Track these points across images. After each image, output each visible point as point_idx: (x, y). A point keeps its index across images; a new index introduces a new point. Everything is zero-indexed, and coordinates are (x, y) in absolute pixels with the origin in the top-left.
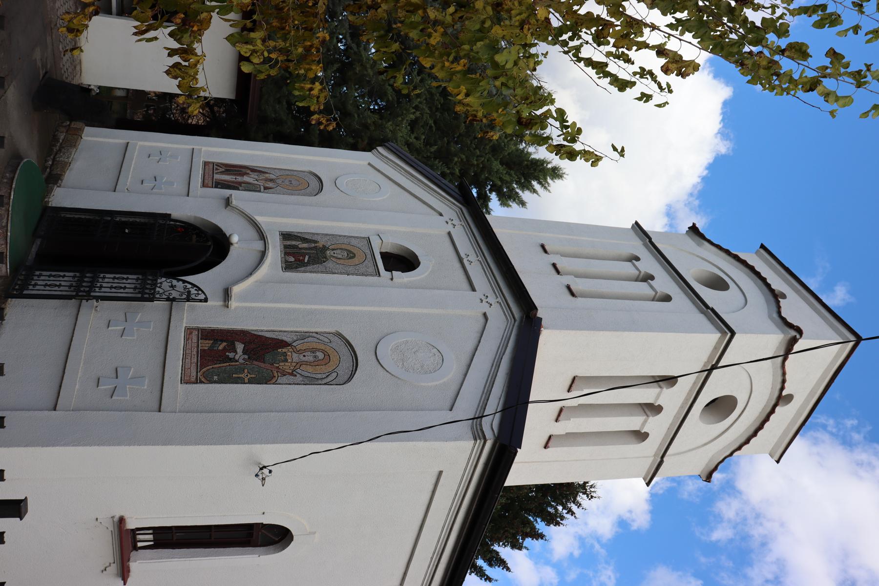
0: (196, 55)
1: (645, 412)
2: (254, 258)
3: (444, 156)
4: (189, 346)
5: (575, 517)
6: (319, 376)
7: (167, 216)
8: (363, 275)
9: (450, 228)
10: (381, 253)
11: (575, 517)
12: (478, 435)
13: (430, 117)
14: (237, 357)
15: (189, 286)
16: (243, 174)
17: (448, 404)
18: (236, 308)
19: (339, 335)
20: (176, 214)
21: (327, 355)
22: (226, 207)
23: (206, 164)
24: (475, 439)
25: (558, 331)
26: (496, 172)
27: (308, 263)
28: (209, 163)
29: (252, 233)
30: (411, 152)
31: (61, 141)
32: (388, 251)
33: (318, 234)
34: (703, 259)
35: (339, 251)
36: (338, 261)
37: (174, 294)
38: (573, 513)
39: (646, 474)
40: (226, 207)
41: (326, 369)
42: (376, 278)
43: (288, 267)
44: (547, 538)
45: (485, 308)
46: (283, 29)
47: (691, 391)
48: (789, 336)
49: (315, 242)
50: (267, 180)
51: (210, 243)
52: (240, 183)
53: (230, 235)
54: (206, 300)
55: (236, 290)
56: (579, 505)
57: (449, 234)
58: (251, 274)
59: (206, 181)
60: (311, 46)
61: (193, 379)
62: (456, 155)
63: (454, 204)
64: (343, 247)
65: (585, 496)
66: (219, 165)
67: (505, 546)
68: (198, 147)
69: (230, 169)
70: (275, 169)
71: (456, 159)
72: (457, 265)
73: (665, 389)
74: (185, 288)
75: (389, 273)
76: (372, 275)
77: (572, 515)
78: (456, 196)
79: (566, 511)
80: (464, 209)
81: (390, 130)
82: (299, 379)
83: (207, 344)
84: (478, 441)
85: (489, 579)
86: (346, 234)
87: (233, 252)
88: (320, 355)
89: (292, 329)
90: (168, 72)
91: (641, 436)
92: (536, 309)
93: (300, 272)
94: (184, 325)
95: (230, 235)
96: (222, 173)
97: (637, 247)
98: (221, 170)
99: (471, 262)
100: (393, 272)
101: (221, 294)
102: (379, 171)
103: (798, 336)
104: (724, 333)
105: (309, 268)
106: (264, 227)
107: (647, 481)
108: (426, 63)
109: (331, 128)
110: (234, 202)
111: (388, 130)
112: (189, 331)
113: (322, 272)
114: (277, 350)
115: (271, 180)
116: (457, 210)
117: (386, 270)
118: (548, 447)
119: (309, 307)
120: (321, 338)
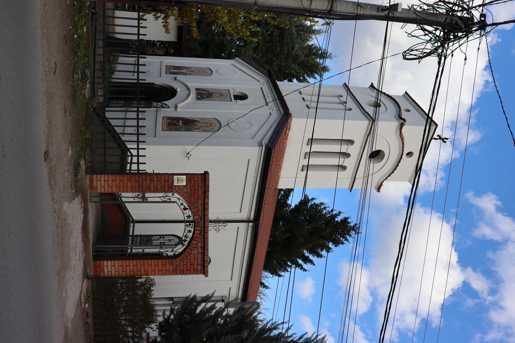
0: (168, 23)
5: (349, 242)
7: (153, 84)
9: (262, 86)
10: (233, 95)
11: (349, 242)
12: (260, 145)
14: (180, 125)
16: (181, 69)
18: (179, 111)
19: (216, 119)
20: (156, 83)
21: (211, 125)
22: (175, 80)
23: (166, 66)
24: (259, 147)
25: (299, 119)
26: (293, 68)
27: (206, 98)
28: (168, 66)
29: (185, 88)
31: (112, 60)
32: (237, 94)
33: (210, 89)
36: (217, 97)
37: (158, 106)
38: (348, 240)
39: (349, 186)
40: (175, 80)
41: (211, 128)
43: (198, 99)
45: (271, 111)
46: (187, 15)
47: (361, 147)
48: (401, 122)
49: (208, 91)
52: (180, 73)
53: (177, 89)
54: (169, 108)
56: (350, 236)
57: (261, 88)
58: (184, 101)
59: (167, 72)
62: (275, 62)
63: (265, 77)
64: (219, 92)
65: (354, 232)
66: (172, 66)
68: (163, 60)
69: (176, 68)
70: (193, 67)
72: (263, 98)
73: (349, 146)
74: (162, 104)
75: (235, 101)
76: (229, 101)
77: (347, 241)
78: (267, 75)
79: (344, 239)
81: (244, 52)
82: (201, 130)
83: (170, 121)
84: (260, 147)
85: (305, 270)
87: (178, 94)
88: (208, 124)
89: (199, 117)
90: (163, 26)
91: (344, 168)
93: (202, 100)
94: (162, 116)
95: (177, 89)
96: (173, 69)
97: (344, 92)
98: (172, 68)
99: (268, 97)
100: (237, 100)
101: (174, 107)
102: (235, 67)
103: (404, 122)
104: (370, 121)
105: (205, 99)
106: (189, 87)
107: (350, 190)
108: (437, 18)
109: (198, 38)
110: (178, 78)
112: (163, 118)
113: (210, 100)
114: (194, 122)
115: (192, 71)
116: (266, 79)
117: (235, 99)
120: (209, 120)
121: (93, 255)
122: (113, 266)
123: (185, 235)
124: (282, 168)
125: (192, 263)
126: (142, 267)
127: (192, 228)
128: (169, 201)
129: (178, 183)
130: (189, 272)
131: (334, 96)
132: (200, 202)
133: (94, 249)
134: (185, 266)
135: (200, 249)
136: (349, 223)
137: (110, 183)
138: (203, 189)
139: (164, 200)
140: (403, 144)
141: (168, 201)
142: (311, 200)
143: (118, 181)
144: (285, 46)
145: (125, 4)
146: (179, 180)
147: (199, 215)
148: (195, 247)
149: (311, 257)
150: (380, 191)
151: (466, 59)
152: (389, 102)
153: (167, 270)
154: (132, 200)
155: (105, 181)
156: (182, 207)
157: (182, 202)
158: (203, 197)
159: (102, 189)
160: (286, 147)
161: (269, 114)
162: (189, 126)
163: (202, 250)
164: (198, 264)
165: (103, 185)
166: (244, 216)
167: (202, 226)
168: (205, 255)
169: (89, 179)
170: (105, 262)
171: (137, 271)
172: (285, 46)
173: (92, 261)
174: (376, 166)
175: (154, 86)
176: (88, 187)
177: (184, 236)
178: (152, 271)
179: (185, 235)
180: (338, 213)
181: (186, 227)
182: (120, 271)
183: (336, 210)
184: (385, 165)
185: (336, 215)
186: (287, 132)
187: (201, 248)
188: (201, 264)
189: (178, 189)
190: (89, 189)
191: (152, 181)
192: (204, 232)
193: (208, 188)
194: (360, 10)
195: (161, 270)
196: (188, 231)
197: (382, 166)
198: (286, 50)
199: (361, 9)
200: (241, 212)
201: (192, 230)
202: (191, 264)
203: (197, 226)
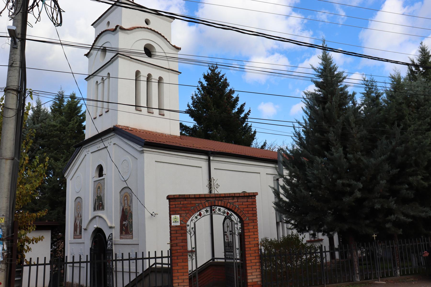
1: (151, 79)
2: (101, 220)
3: (68, 146)
4: (128, 238)
5: (224, 74)
6: (130, 198)
8: (104, 184)
9: (90, 153)
10: (99, 177)
11: (224, 74)
12: (142, 152)
13: (53, 152)
14: (127, 223)
15: (109, 239)
16: (77, 225)
17: (136, 159)
23: (74, 238)
24: (144, 153)
27: (102, 202)
29: (94, 221)
30: (67, 160)
32: (98, 174)
33: (94, 199)
34: (96, 54)
35: (98, 192)
37: (111, 244)
38: (223, 75)
42: (105, 180)
43: (103, 209)
44: (231, 88)
45: (112, 144)
46: (26, 222)
47: (142, 64)
49: (96, 200)
50: (78, 216)
51: (98, 234)
52: (80, 226)
53: (95, 228)
54: (112, 234)
55: (109, 225)
56: (219, 73)
57: (92, 153)
58: (105, 220)
60: (29, 216)
61: (132, 236)
62: (68, 142)
63: (82, 150)
64: (97, 190)
65: (216, 70)
66: (74, 234)
67: (237, 104)
69: (75, 230)
71: (69, 142)
72: (101, 151)
73: (141, 75)
74: (109, 240)
76: (104, 181)
77: (224, 76)
78: (79, 148)
80: (83, 147)
82: (131, 205)
83: (124, 232)
85: (249, 111)
86: (93, 189)
87: (100, 226)
88: (125, 198)
90: (37, 243)
91: (160, 80)
93: (104, 205)
95: (95, 228)
96: (77, 232)
97: (94, 80)
98: (76, 233)
99: (99, 147)
103: (119, 27)
104: (118, 57)
107: (179, 74)
110: (85, 227)
111: (59, 171)
113: (104, 197)
115: (78, 215)
117: (103, 176)
118: (164, 114)
119: (113, 202)
122: (252, 274)
123: (222, 214)
124: (162, 133)
125: (246, 206)
127: (216, 208)
128: (194, 228)
129: (178, 222)
130: (254, 208)
131: (97, 88)
134: (249, 212)
136: (208, 74)
137: (181, 281)
138: (182, 200)
139: (193, 233)
140: (138, 28)
141: (194, 230)
142: (189, 107)
143: (178, 274)
144: (52, 133)
146: (176, 221)
148: (233, 204)
149: (238, 106)
153: (254, 227)
155: (178, 286)
156: (199, 217)
157: (194, 217)
158: (190, 200)
161: (115, 145)
162: (127, 215)
164: (247, 201)
166: (204, 164)
167: (214, 199)
170: (249, 281)
171: (255, 253)
177: (224, 214)
178: (254, 241)
179: (222, 214)
180: (200, 84)
185: (202, 85)
186: (130, 129)
187: (233, 199)
189: (183, 222)
191: (177, 244)
192: (220, 197)
194: (16, 64)
196: (219, 211)
197: (158, 46)
198: (56, 132)
199: (15, 63)
200: (201, 167)
201: (218, 207)
203: (215, 203)
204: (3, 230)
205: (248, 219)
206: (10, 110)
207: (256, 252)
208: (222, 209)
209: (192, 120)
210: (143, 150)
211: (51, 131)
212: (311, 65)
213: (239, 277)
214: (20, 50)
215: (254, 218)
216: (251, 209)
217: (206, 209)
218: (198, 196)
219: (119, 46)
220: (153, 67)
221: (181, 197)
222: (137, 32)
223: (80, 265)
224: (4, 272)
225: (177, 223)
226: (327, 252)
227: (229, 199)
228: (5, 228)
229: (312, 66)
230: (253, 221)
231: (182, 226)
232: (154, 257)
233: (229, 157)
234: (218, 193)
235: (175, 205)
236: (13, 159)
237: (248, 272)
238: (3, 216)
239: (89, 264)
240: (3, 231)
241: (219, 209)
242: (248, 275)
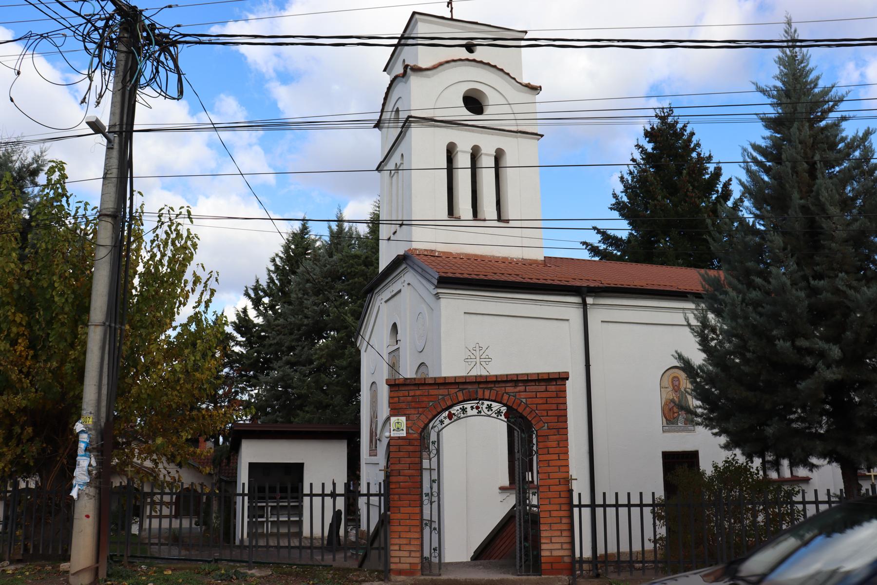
12: (438, 298)
24: (440, 298)
38: (685, 126)
57: (386, 302)
73: (458, 149)
77: (686, 127)
91: (499, 156)
92: (398, 255)
103: (409, 67)
116: (376, 296)
121: (534, 575)
122: (551, 540)
123: (495, 416)
124: (504, 256)
125: (544, 401)
126: (553, 488)
127: (483, 404)
128: (436, 443)
129: (403, 430)
130: (562, 405)
131: (392, 183)
132: (434, 392)
133: (522, 572)
134: (550, 413)
135: (518, 389)
136: (652, 128)
137: (404, 541)
138: (412, 388)
139: (435, 452)
140: (448, 62)
141: (436, 445)
142: (616, 199)
143: (400, 529)
144: (353, 269)
145: (281, 521)
146: (398, 429)
147: (456, 393)
148: (515, 396)
149: (719, 187)
150: (538, 85)
151: (170, 7)
152: (393, 95)
153: (559, 445)
154: (435, 505)
155: (400, 550)
156: (447, 421)
157: (438, 422)
158: (426, 387)
159: (413, 554)
160: (465, 254)
161: (410, 286)
163: (520, 385)
164: (546, 391)
165: (406, 554)
166: (574, 314)
167: (476, 386)
168: (526, 379)
169: (397, 577)
170: (543, 553)
171: (560, 497)
172: (353, 269)
173: (543, 576)
174: (492, 98)
175: (844, 495)
176: (411, 578)
177: (498, 416)
178: (559, 472)
179: (495, 416)
180: (639, 149)
181: (483, 413)
182: (560, 528)
183: (632, 154)
184: (489, 86)
185: (643, 151)
186: (437, 254)
187: (516, 386)
188: (546, 385)
189: (412, 430)
190: (415, 577)
191: (399, 472)
192: (487, 382)
193: (409, 380)
194: (111, 174)
195: (559, 456)
196: (488, 411)
197: (492, 89)
198: (359, 268)
199: (109, 172)
200: (568, 320)
201: (486, 403)
202: (545, 402)
203: (477, 395)
204: (91, 436)
205: (546, 427)
206: (101, 247)
207: (563, 495)
208: (496, 406)
209: (624, 224)
210: (438, 293)
211: (352, 266)
212: (753, 83)
213: (526, 543)
214: (118, 150)
215: (561, 425)
216: (554, 407)
217: (461, 406)
218: (442, 381)
219: (412, 103)
220: (482, 131)
221: (408, 382)
222: (446, 71)
223: (368, 500)
224: (93, 499)
225: (401, 432)
226: (307, 495)
227: (508, 385)
228: (93, 432)
229: (756, 84)
230: (558, 431)
231: (410, 437)
232: (321, 493)
233: (648, 296)
234: (487, 374)
235: (398, 397)
236: (104, 324)
237: (542, 535)
238: (91, 413)
239: (246, 498)
240: (90, 438)
241: (488, 405)
242: (543, 541)
